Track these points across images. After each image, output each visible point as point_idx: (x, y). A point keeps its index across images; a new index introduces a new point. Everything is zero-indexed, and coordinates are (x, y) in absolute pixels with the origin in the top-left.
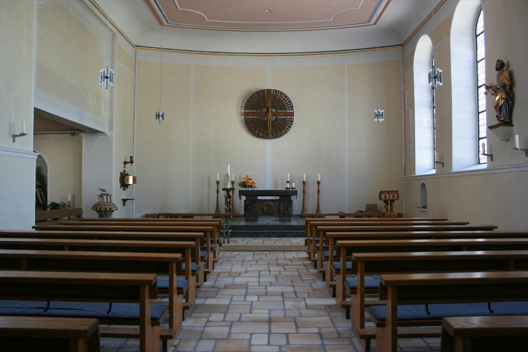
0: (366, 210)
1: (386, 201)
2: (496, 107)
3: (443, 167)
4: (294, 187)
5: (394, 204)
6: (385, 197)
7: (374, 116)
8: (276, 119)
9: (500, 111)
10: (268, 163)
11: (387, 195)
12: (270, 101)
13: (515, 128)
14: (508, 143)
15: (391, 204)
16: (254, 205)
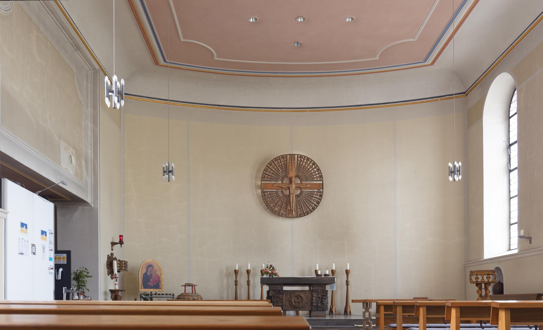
1: (478, 284)
3: (530, 243)
7: (448, 172)
8: (302, 192)
12: (294, 170)
15: (486, 288)
16: (280, 296)
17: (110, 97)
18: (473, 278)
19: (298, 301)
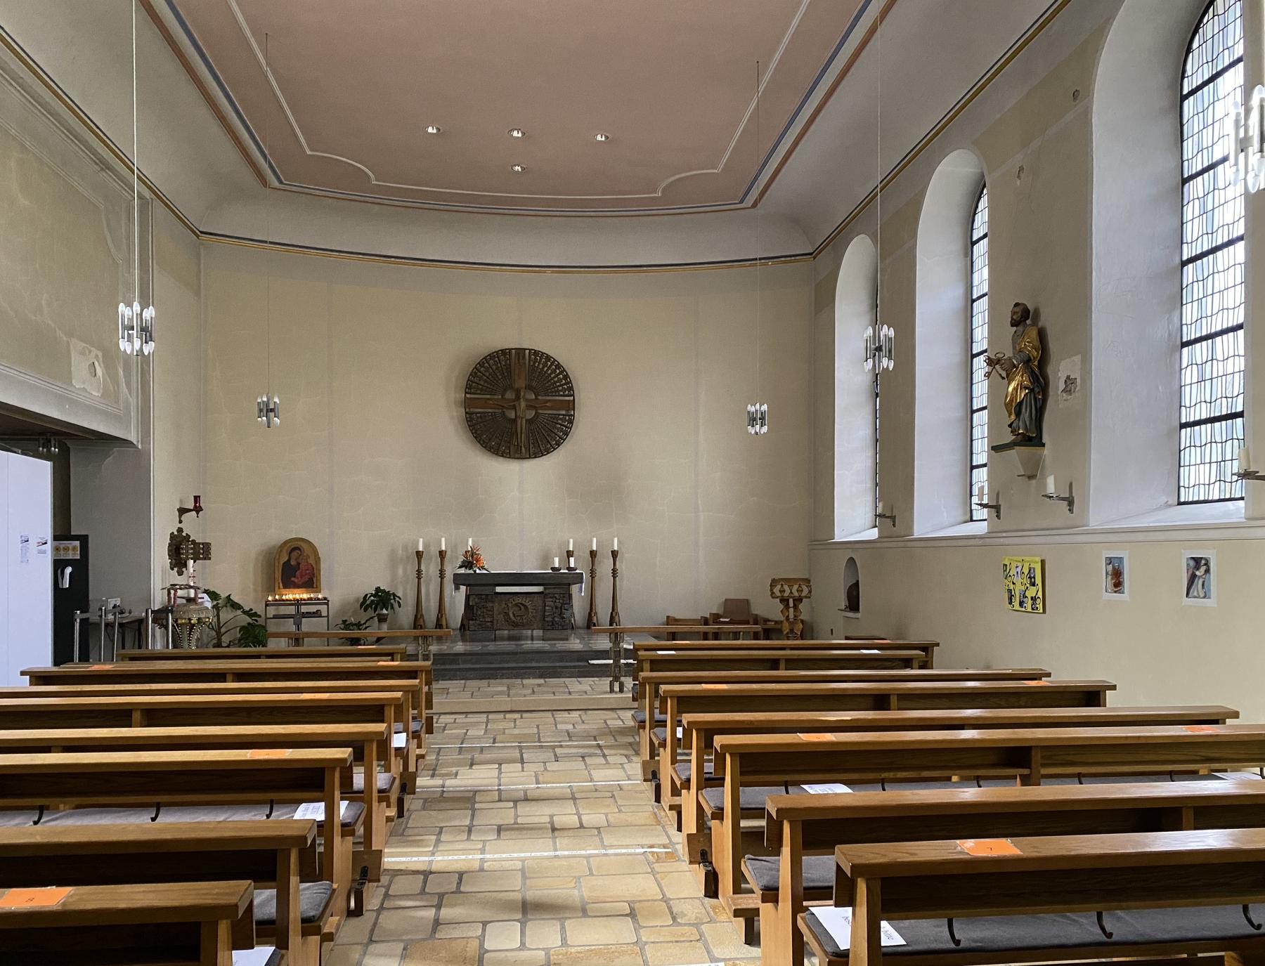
0: (725, 611)
1: (784, 601)
2: (1008, 405)
4: (572, 565)
5: (801, 606)
6: (782, 591)
8: (537, 415)
9: (1018, 414)
10: (522, 516)
11: (786, 587)
13: (1046, 451)
14: (1034, 482)
15: (795, 607)
17: (130, 339)
18: (777, 590)
19: (519, 613)
